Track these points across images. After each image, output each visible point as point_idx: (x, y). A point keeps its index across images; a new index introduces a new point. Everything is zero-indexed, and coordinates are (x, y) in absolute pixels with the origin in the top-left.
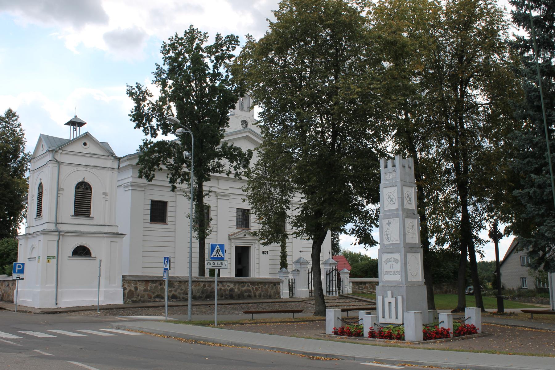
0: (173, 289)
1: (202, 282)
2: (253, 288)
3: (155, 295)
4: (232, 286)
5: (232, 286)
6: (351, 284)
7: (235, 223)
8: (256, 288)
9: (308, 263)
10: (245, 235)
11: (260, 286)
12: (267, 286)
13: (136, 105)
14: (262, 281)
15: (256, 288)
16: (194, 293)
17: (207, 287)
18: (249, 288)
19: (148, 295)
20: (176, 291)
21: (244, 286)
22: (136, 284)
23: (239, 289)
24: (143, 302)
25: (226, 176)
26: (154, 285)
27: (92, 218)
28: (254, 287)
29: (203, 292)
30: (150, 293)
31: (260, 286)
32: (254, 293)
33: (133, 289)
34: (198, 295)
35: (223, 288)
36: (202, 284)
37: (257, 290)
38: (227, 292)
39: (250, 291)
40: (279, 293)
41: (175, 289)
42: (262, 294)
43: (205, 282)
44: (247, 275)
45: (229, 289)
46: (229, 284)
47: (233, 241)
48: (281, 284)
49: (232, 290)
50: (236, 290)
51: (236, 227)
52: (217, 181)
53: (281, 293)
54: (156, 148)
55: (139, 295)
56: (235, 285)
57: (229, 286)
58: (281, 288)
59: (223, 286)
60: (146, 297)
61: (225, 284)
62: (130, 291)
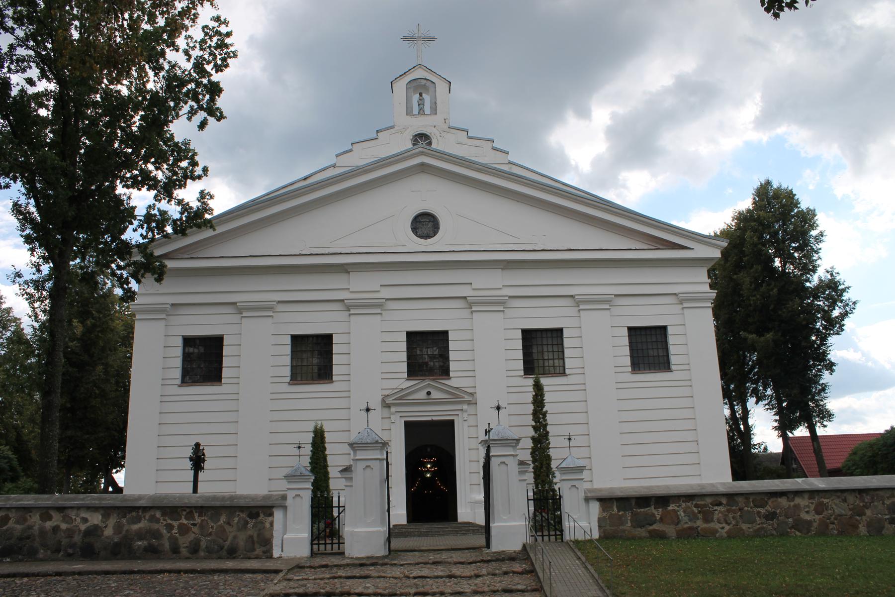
2: (170, 527)
4: (95, 519)
5: (95, 519)
8: (181, 526)
11: (198, 520)
12: (223, 519)
15: (181, 526)
17: (11, 524)
18: (155, 526)
21: (138, 520)
23: (118, 528)
28: (175, 524)
35: (64, 526)
37: (184, 530)
38: (77, 538)
39: (157, 535)
42: (203, 544)
43: (9, 509)
45: (83, 527)
46: (84, 515)
48: (278, 515)
49: (93, 531)
50: (109, 532)
51: (630, 369)
52: (345, 276)
53: (276, 543)
57: (85, 520)
59: (67, 519)
61: (72, 514)
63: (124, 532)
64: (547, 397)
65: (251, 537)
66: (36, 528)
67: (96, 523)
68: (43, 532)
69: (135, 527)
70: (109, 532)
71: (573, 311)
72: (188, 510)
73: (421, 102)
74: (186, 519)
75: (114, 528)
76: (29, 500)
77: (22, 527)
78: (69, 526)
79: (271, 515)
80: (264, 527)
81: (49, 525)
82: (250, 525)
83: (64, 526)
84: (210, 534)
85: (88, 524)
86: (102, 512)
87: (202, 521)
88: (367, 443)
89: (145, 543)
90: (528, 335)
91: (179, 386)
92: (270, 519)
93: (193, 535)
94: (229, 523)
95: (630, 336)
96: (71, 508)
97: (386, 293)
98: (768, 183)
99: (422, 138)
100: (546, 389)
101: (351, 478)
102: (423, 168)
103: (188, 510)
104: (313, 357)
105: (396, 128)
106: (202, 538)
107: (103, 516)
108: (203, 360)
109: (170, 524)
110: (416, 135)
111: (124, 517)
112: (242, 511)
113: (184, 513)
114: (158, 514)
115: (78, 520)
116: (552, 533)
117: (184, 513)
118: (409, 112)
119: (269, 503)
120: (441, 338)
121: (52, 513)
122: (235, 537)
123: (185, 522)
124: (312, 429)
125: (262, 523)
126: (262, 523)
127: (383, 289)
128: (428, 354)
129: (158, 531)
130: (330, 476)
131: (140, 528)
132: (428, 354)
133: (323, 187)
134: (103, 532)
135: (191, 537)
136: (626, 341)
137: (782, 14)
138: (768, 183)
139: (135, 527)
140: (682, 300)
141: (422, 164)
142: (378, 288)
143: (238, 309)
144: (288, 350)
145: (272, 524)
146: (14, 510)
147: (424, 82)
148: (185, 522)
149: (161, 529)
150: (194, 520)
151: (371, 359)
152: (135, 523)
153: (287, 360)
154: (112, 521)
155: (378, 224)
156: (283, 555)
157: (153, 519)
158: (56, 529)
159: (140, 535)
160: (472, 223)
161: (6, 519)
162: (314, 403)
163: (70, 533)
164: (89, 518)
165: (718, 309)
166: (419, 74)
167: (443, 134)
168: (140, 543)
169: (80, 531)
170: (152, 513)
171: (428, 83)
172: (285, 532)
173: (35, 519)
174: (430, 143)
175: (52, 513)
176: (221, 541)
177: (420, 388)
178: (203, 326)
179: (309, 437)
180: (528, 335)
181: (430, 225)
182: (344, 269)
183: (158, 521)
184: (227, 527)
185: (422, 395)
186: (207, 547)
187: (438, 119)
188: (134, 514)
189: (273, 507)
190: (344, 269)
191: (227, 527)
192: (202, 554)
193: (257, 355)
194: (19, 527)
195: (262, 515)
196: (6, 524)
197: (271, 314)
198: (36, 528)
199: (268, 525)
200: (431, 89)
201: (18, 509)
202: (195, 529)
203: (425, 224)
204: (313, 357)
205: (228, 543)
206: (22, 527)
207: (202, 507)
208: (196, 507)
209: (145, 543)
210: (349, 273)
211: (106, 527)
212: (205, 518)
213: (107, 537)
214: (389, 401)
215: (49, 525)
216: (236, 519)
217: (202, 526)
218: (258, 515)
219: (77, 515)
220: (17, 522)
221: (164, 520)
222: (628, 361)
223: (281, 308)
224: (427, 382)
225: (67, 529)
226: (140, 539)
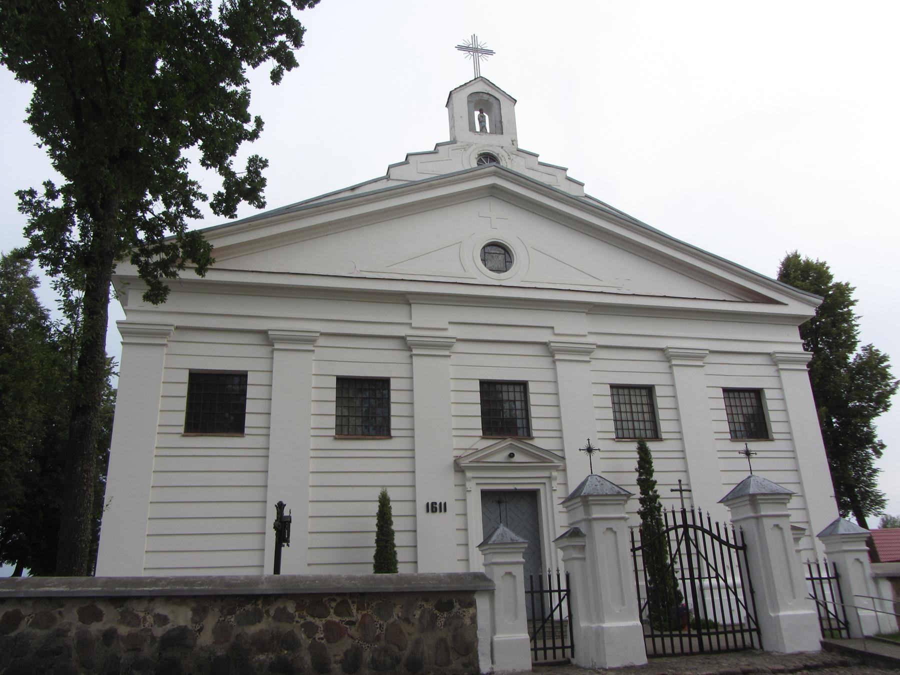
2: (310, 629)
4: (182, 617)
5: (182, 617)
6: (887, 590)
7: (478, 422)
8: (329, 627)
9: (629, 495)
10: (511, 455)
11: (357, 616)
12: (397, 612)
13: (223, 191)
14: (222, 590)
15: (329, 627)
17: (24, 627)
18: (286, 627)
21: (256, 617)
23: (221, 631)
25: (223, 220)
28: (319, 622)
31: (357, 616)
32: (315, 648)
35: (123, 630)
37: (333, 633)
38: (147, 651)
39: (290, 642)
42: (367, 656)
43: (20, 600)
44: (83, 556)
45: (159, 632)
46: (161, 609)
47: (469, 474)
48: (482, 604)
49: (178, 639)
50: (206, 639)
51: (480, 433)
52: (405, 308)
53: (483, 648)
54: (141, 235)
56: (200, 612)
57: (162, 620)
58: (483, 622)
59: (128, 618)
61: (139, 609)
63: (232, 639)
64: (656, 465)
65: (442, 641)
66: (73, 633)
67: (182, 623)
68: (84, 642)
69: (253, 629)
70: (206, 639)
72: (339, 600)
73: (482, 121)
74: (336, 613)
75: (214, 632)
76: (52, 589)
77: (45, 632)
78: (134, 630)
79: (472, 604)
80: (463, 624)
81: (96, 628)
82: (441, 622)
83: (123, 630)
84: (378, 638)
85: (168, 627)
86: (193, 605)
87: (364, 616)
88: (607, 495)
89: (272, 656)
91: (183, 436)
92: (471, 611)
93: (350, 641)
94: (407, 620)
95: (338, 389)
96: (139, 598)
97: (454, 332)
98: (796, 256)
99: (487, 158)
100: (653, 455)
101: (583, 548)
102: (494, 192)
103: (339, 600)
104: (364, 406)
105: (459, 144)
106: (365, 646)
107: (195, 611)
108: (216, 404)
109: (311, 623)
110: (481, 155)
111: (232, 612)
112: (427, 600)
113: (334, 604)
114: (291, 608)
115: (150, 619)
116: (694, 632)
117: (334, 604)
118: (472, 128)
119: (469, 587)
121: (101, 607)
122: (418, 642)
123: (337, 619)
125: (459, 618)
126: (458, 617)
127: (450, 327)
128: (503, 410)
129: (291, 635)
131: (261, 631)
132: (503, 410)
133: (379, 200)
134: (195, 639)
135: (346, 644)
136: (184, 390)
138: (796, 256)
139: (253, 629)
140: (774, 360)
141: (493, 187)
142: (447, 326)
143: (267, 338)
144: (332, 395)
145: (474, 619)
146: (30, 603)
147: (487, 97)
148: (337, 619)
149: (297, 631)
150: (350, 614)
151: (439, 409)
152: (252, 623)
153: (332, 408)
154: (211, 622)
155: (442, 248)
156: (496, 669)
157: (282, 616)
158: (109, 636)
159: (261, 644)
160: (548, 260)
161: (13, 620)
162: (369, 466)
163: (134, 643)
164: (171, 617)
165: (810, 373)
166: (480, 87)
167: (513, 157)
168: (262, 657)
169: (153, 638)
170: (280, 604)
171: (491, 100)
172: (494, 632)
173: (70, 619)
174: (499, 163)
175: (101, 607)
176: (396, 650)
177: (499, 449)
178: (219, 358)
179: (375, 508)
181: (501, 257)
182: (405, 299)
183: (290, 619)
184: (405, 627)
185: (502, 457)
186: (373, 660)
187: (504, 140)
188: (249, 607)
189: (473, 592)
190: (405, 299)
191: (405, 627)
193: (293, 398)
194: (37, 632)
195: (457, 606)
196: (15, 626)
197: (311, 348)
198: (73, 633)
199: (467, 621)
200: (495, 106)
201: (38, 600)
202: (352, 631)
203: (498, 254)
204: (364, 406)
205: (406, 653)
206: (45, 632)
207: (363, 594)
208: (352, 595)
209: (272, 656)
210: (410, 305)
211: (200, 631)
212: (370, 612)
213: (202, 649)
214: (464, 463)
215: (96, 628)
216: (418, 613)
217: (364, 625)
218: (449, 606)
219: (148, 611)
220: (35, 624)
221: (301, 617)
223: (322, 341)
224: (509, 441)
225: (130, 635)
226: (262, 650)
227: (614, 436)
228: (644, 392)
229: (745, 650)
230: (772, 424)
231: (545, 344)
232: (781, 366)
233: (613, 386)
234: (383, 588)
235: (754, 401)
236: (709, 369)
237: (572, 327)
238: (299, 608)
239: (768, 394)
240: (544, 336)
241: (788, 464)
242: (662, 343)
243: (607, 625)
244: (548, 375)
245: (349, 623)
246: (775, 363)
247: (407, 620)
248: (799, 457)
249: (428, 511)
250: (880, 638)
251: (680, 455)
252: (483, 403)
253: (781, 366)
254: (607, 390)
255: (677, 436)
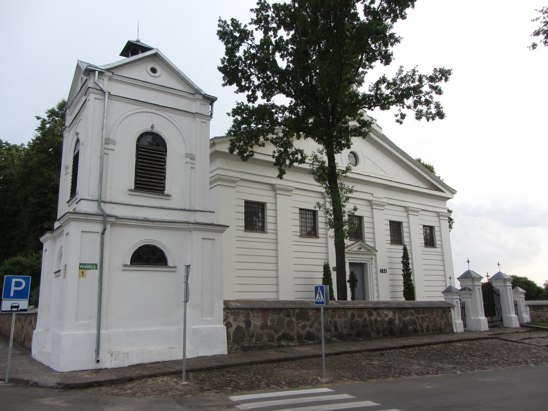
0: (308, 323)
1: (350, 309)
3: (280, 334)
4: (390, 314)
16: (340, 330)
18: (413, 318)
19: (269, 335)
20: (311, 326)
21: (406, 315)
22: (248, 316)
24: (261, 348)
26: (276, 317)
27: (168, 195)
28: (419, 316)
29: (352, 327)
30: (272, 332)
33: (243, 325)
34: (345, 331)
35: (379, 319)
36: (349, 313)
40: (450, 325)
41: (310, 322)
42: (430, 327)
46: (386, 312)
49: (391, 321)
50: (397, 322)
51: (243, 228)
55: (252, 337)
56: (394, 313)
57: (386, 315)
60: (265, 339)
61: (381, 312)
62: (238, 328)
71: (271, 194)
79: (450, 311)
90: (248, 204)
95: (246, 207)
96: (381, 308)
120: (262, 206)
121: (372, 311)
122: (440, 323)
124: (323, 264)
129: (415, 320)
130: (403, 293)
136: (243, 210)
137: (433, 72)
175: (372, 311)
179: (322, 269)
180: (248, 204)
185: (356, 249)
186: (432, 328)
192: (431, 332)
205: (438, 326)
215: (373, 318)
222: (243, 223)
226: (410, 325)
227: (299, 234)
228: (249, 205)
229: (441, 331)
230: (268, 224)
231: (369, 201)
232: (441, 218)
233: (300, 209)
234: (408, 306)
235: (312, 216)
236: (386, 211)
237: (379, 194)
238: (415, 312)
239: (365, 219)
240: (369, 197)
241: (273, 246)
242: (406, 205)
243: (480, 318)
244: (369, 214)
245: (426, 317)
246: (439, 216)
247: (438, 316)
248: (279, 243)
249: (80, 264)
250: (527, 323)
251: (441, 254)
252: (246, 213)
253: (441, 218)
254: (298, 211)
255: (274, 232)
